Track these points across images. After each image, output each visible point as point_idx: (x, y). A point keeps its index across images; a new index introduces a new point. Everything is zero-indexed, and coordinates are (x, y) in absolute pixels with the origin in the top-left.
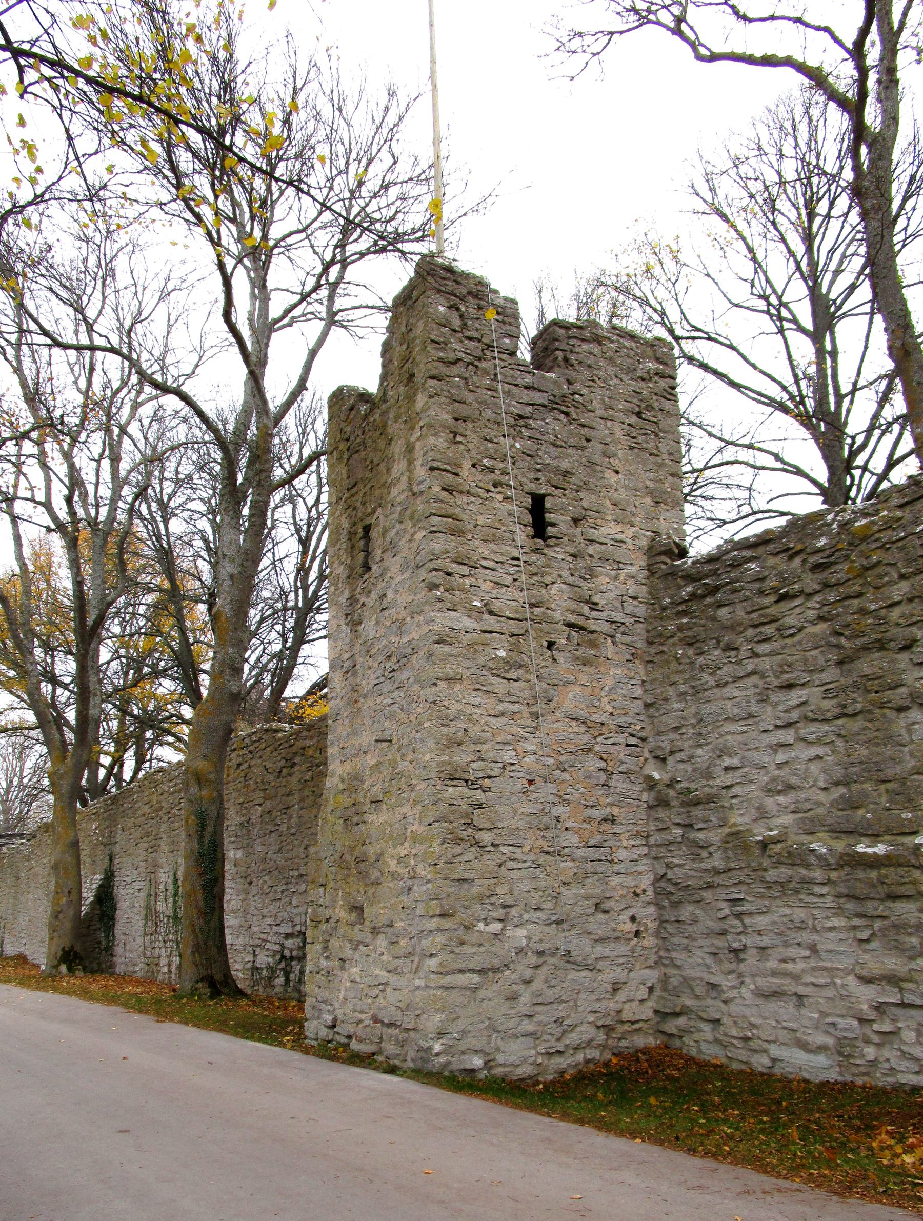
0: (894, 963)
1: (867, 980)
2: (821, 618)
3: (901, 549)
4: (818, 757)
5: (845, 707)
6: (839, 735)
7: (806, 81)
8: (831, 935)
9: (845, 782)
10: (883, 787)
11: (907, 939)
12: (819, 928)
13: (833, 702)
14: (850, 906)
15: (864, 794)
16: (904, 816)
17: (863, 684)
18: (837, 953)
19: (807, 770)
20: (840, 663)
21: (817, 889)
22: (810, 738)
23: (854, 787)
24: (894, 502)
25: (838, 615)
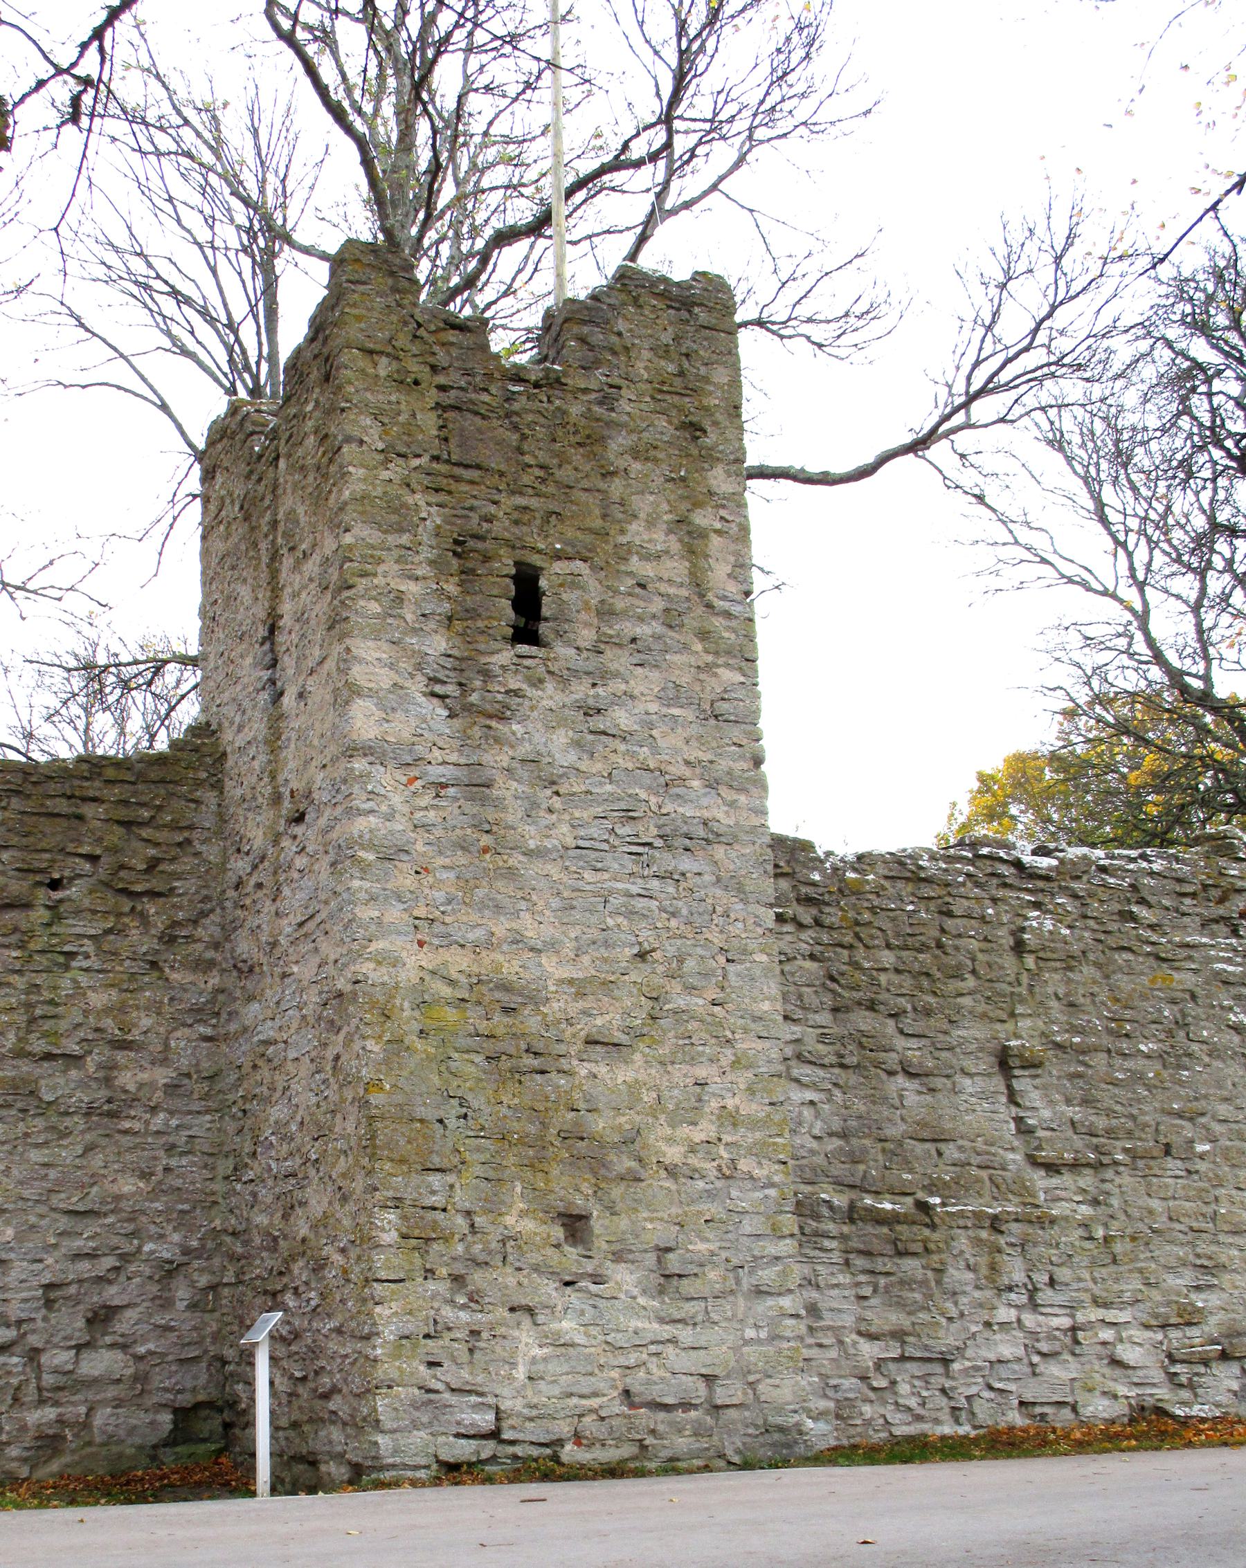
0: (896, 1319)
1: (872, 1337)
2: (812, 957)
3: (893, 920)
4: (812, 1103)
5: (842, 1056)
6: (835, 1085)
7: (925, 431)
8: (835, 1292)
9: (844, 1135)
10: (879, 1145)
11: (910, 1295)
12: (822, 1284)
13: (830, 1048)
14: (859, 1262)
15: (864, 1150)
16: (905, 1176)
17: (862, 1040)
18: (840, 1311)
19: (800, 1113)
20: (835, 1010)
21: (827, 1243)
22: (805, 1080)
23: (854, 1141)
24: (882, 871)
25: (829, 959)
